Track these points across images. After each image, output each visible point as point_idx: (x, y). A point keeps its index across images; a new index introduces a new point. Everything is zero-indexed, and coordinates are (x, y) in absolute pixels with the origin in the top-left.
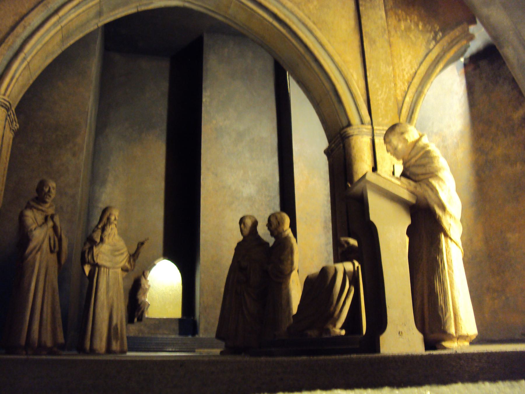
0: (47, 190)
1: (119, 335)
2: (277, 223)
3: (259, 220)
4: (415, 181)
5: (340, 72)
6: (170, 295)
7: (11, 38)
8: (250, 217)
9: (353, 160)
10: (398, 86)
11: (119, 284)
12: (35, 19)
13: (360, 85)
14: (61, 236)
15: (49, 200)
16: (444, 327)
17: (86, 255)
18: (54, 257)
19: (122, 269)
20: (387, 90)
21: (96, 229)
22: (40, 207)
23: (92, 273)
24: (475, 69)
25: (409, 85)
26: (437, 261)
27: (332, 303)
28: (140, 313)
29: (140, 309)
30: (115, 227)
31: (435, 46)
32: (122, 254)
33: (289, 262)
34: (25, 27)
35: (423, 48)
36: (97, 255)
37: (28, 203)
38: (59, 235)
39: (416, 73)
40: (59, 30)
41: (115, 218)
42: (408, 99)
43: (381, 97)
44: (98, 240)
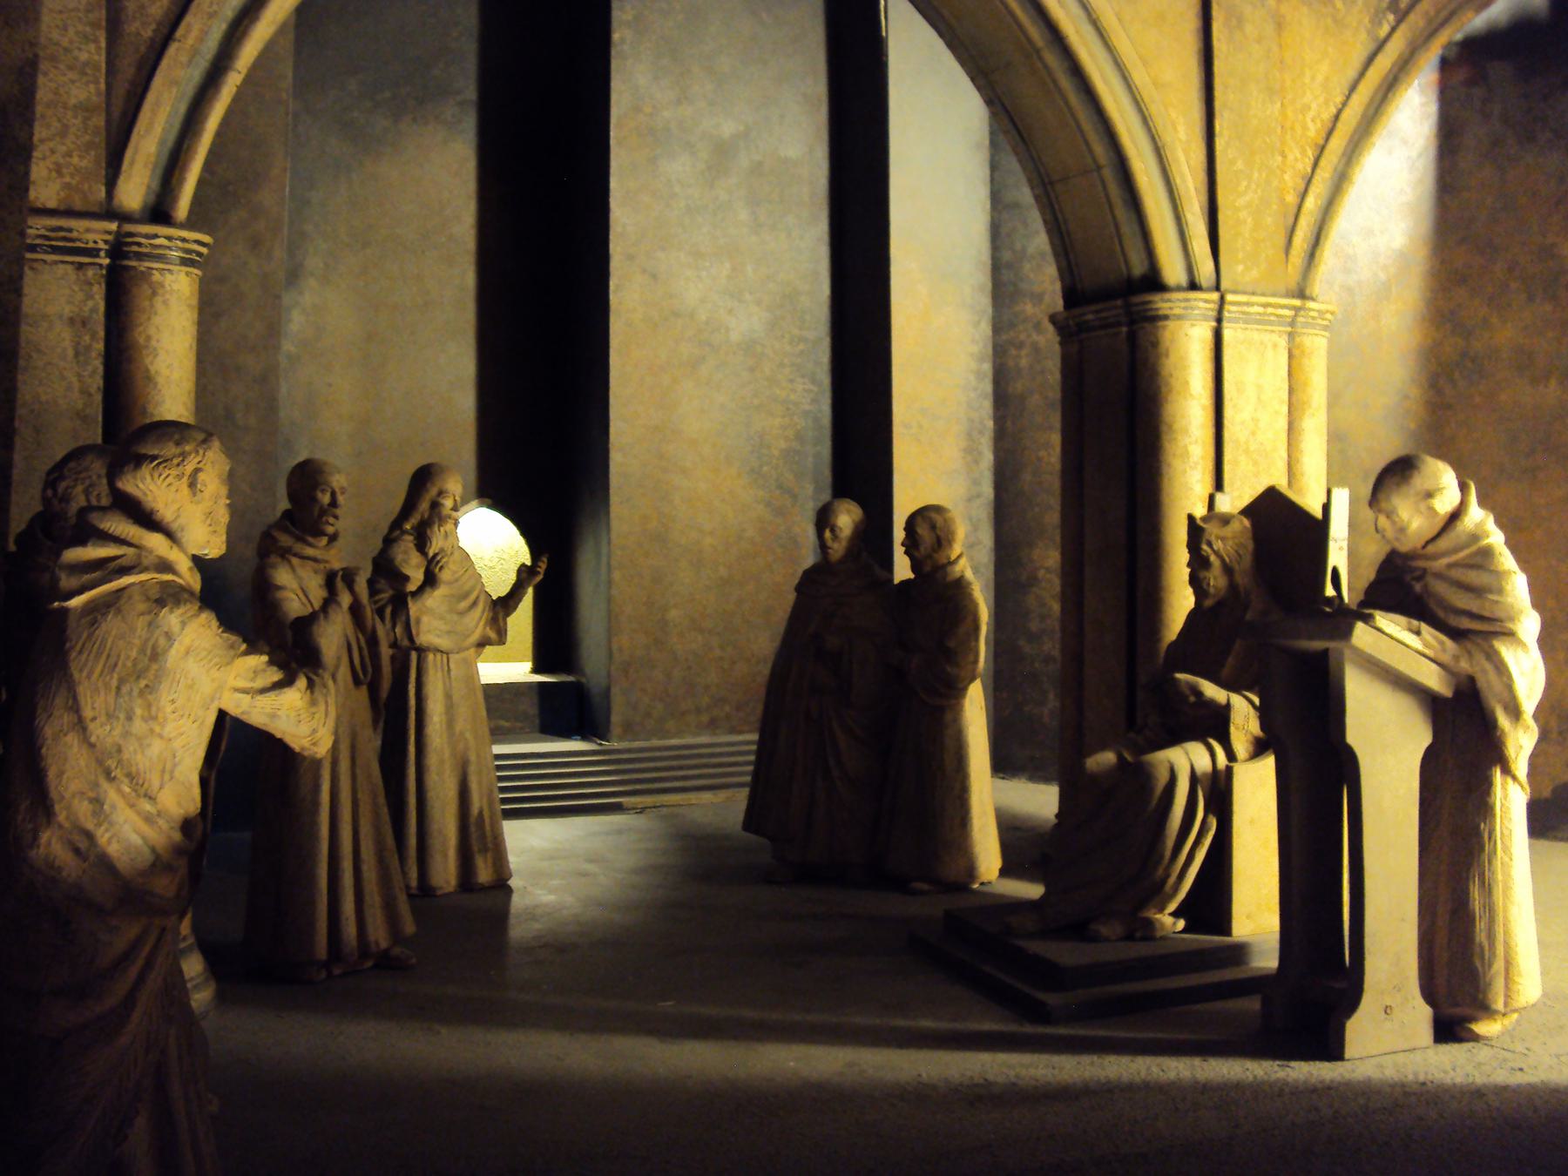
1: (489, 839)
2: (935, 540)
4: (1456, 634)
5: (1145, 121)
9: (1164, 389)
10: (1290, 157)
13: (1192, 163)
14: (374, 631)
16: (1485, 993)
20: (1264, 175)
22: (310, 551)
24: (1470, 83)
25: (1316, 156)
26: (1477, 834)
27: (1162, 857)
31: (1393, 29)
35: (1363, 36)
39: (1337, 117)
42: (1311, 203)
43: (1247, 198)
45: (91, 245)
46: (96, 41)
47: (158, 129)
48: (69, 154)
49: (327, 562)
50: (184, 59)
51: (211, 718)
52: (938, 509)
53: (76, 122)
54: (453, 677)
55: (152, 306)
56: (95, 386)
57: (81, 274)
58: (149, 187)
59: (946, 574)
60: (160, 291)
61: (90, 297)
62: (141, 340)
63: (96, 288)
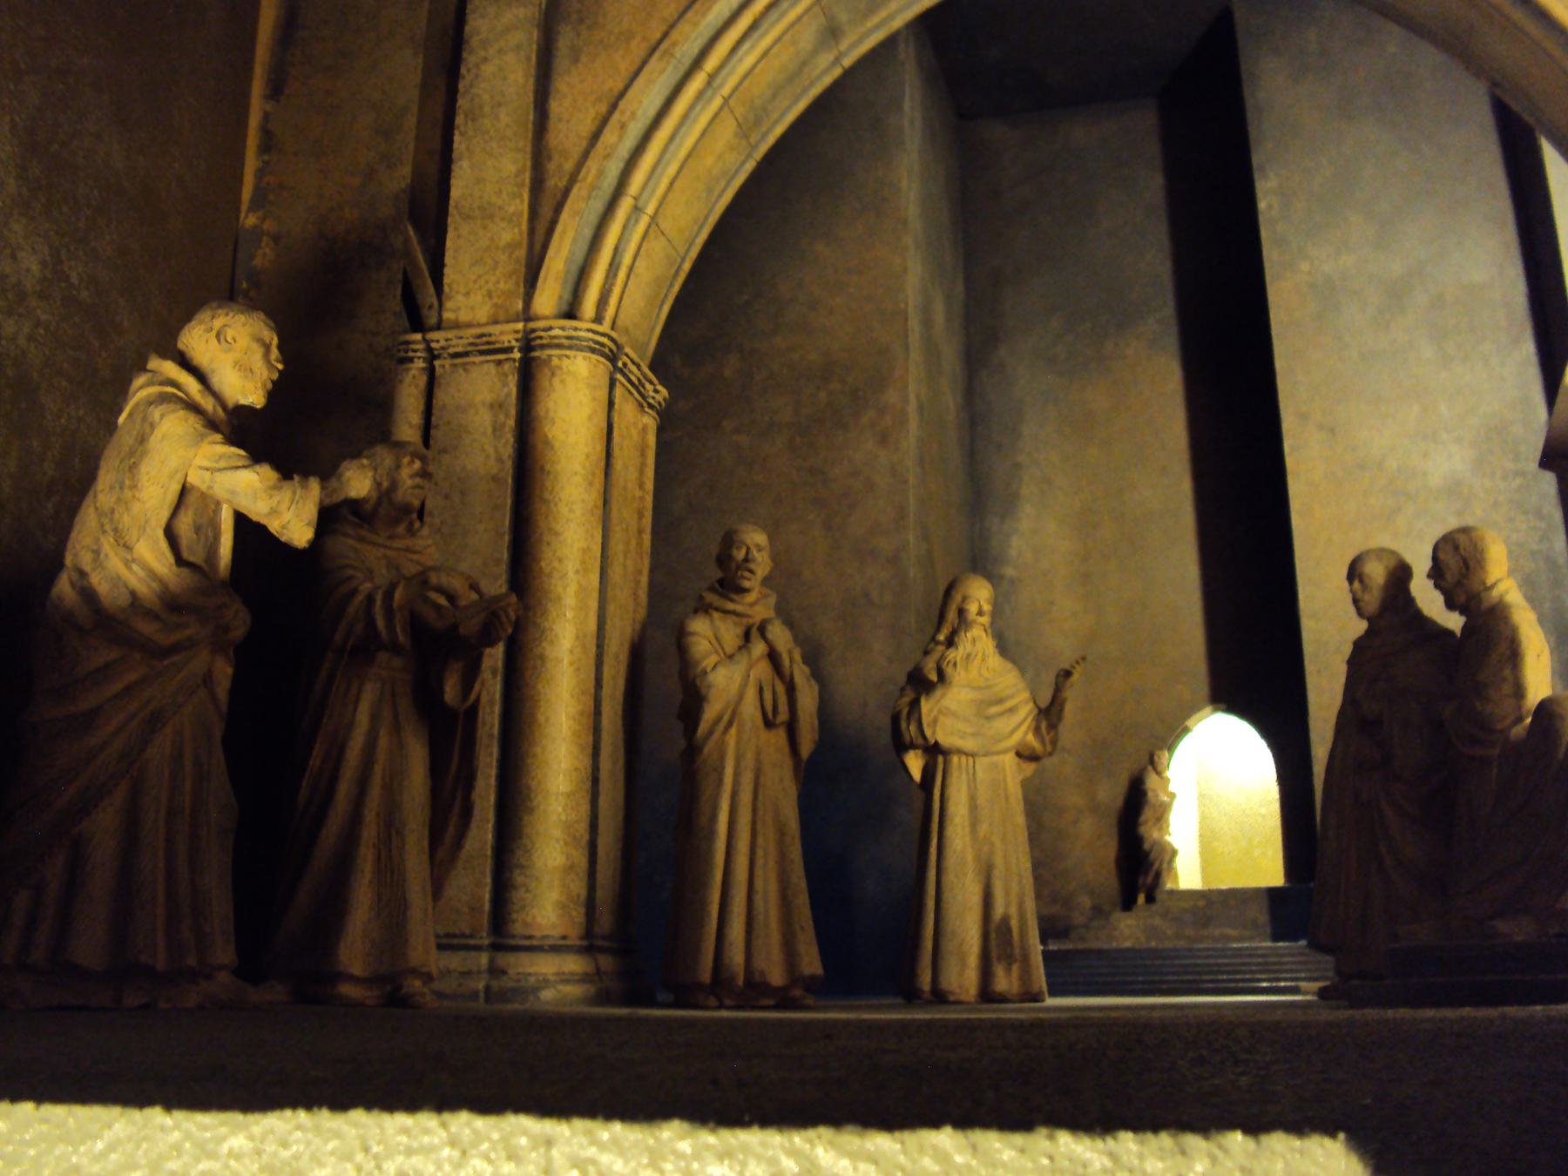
0: (740, 555)
3: (1409, 558)
6: (1263, 816)
7: (592, 165)
8: (1381, 553)
11: (1007, 798)
12: (645, 99)
15: (753, 583)
17: (903, 725)
18: (779, 737)
19: (1018, 754)
21: (932, 645)
22: (731, 606)
23: (928, 772)
28: (1150, 879)
29: (1152, 864)
30: (984, 634)
32: (1012, 710)
33: (1507, 689)
34: (623, 126)
36: (935, 721)
37: (701, 598)
38: (787, 673)
40: (721, 109)
41: (980, 606)
44: (934, 677)
45: (506, 344)
46: (521, 196)
47: (565, 252)
48: (498, 282)
49: (749, 616)
50: (584, 193)
51: (175, 488)
52: (1465, 530)
53: (502, 257)
54: (978, 779)
55: (551, 384)
56: (507, 454)
57: (500, 369)
58: (560, 297)
59: (1480, 602)
60: (558, 372)
61: (505, 384)
62: (542, 414)
63: (510, 377)
